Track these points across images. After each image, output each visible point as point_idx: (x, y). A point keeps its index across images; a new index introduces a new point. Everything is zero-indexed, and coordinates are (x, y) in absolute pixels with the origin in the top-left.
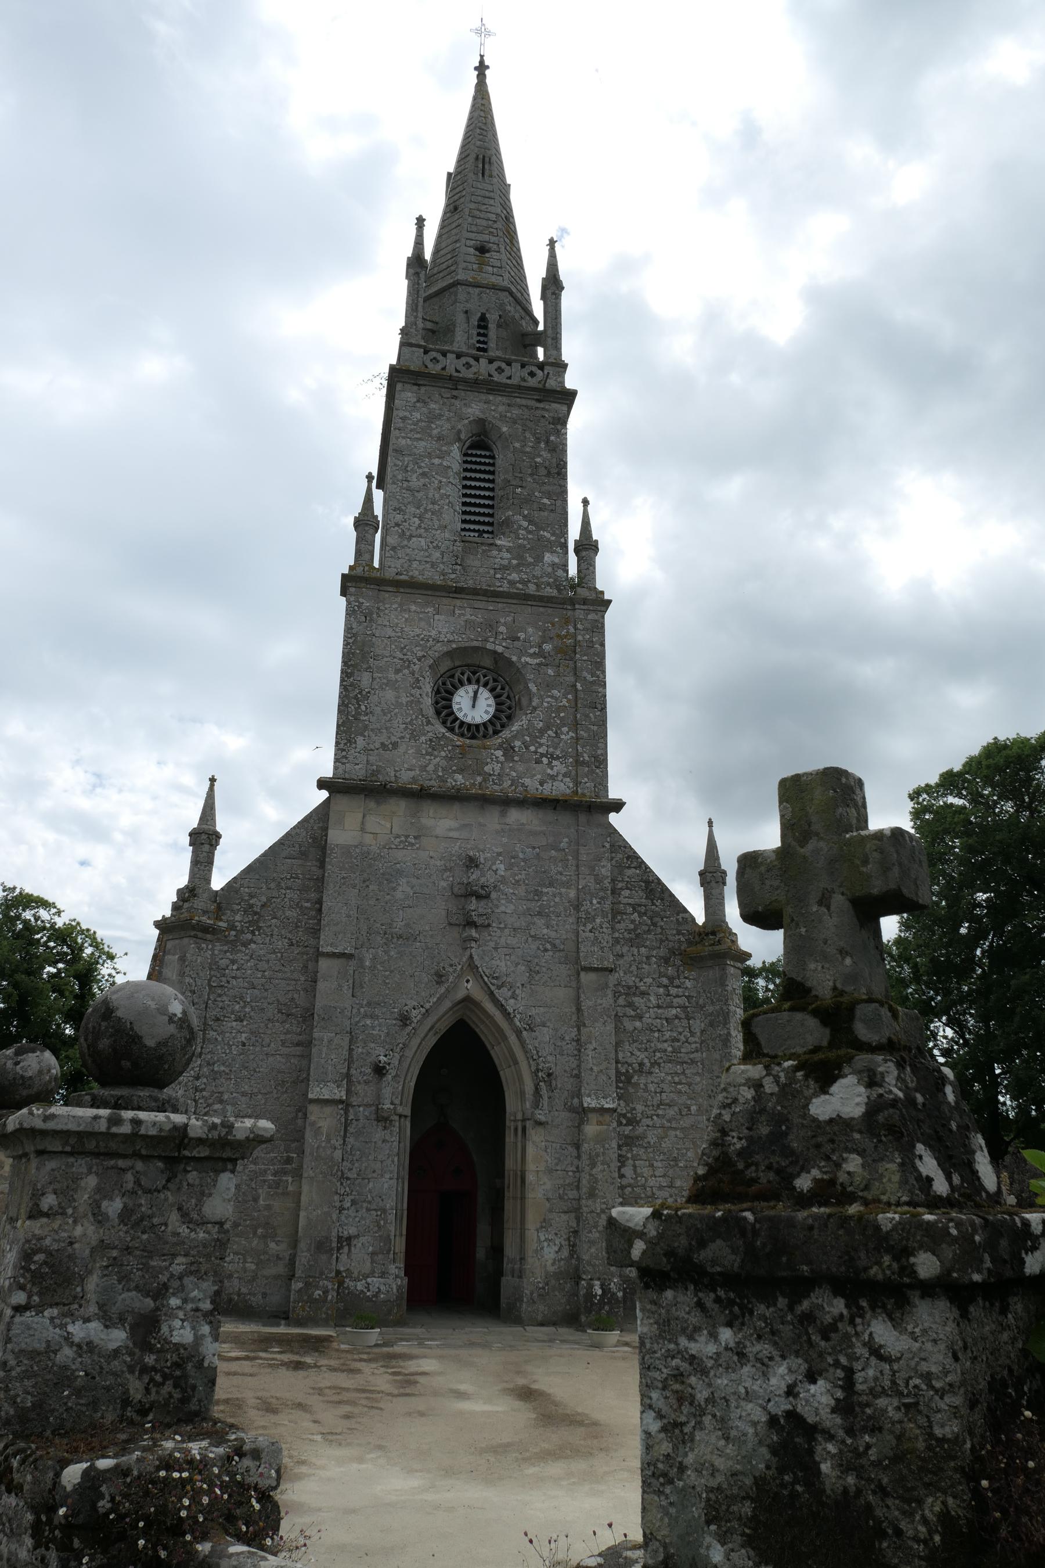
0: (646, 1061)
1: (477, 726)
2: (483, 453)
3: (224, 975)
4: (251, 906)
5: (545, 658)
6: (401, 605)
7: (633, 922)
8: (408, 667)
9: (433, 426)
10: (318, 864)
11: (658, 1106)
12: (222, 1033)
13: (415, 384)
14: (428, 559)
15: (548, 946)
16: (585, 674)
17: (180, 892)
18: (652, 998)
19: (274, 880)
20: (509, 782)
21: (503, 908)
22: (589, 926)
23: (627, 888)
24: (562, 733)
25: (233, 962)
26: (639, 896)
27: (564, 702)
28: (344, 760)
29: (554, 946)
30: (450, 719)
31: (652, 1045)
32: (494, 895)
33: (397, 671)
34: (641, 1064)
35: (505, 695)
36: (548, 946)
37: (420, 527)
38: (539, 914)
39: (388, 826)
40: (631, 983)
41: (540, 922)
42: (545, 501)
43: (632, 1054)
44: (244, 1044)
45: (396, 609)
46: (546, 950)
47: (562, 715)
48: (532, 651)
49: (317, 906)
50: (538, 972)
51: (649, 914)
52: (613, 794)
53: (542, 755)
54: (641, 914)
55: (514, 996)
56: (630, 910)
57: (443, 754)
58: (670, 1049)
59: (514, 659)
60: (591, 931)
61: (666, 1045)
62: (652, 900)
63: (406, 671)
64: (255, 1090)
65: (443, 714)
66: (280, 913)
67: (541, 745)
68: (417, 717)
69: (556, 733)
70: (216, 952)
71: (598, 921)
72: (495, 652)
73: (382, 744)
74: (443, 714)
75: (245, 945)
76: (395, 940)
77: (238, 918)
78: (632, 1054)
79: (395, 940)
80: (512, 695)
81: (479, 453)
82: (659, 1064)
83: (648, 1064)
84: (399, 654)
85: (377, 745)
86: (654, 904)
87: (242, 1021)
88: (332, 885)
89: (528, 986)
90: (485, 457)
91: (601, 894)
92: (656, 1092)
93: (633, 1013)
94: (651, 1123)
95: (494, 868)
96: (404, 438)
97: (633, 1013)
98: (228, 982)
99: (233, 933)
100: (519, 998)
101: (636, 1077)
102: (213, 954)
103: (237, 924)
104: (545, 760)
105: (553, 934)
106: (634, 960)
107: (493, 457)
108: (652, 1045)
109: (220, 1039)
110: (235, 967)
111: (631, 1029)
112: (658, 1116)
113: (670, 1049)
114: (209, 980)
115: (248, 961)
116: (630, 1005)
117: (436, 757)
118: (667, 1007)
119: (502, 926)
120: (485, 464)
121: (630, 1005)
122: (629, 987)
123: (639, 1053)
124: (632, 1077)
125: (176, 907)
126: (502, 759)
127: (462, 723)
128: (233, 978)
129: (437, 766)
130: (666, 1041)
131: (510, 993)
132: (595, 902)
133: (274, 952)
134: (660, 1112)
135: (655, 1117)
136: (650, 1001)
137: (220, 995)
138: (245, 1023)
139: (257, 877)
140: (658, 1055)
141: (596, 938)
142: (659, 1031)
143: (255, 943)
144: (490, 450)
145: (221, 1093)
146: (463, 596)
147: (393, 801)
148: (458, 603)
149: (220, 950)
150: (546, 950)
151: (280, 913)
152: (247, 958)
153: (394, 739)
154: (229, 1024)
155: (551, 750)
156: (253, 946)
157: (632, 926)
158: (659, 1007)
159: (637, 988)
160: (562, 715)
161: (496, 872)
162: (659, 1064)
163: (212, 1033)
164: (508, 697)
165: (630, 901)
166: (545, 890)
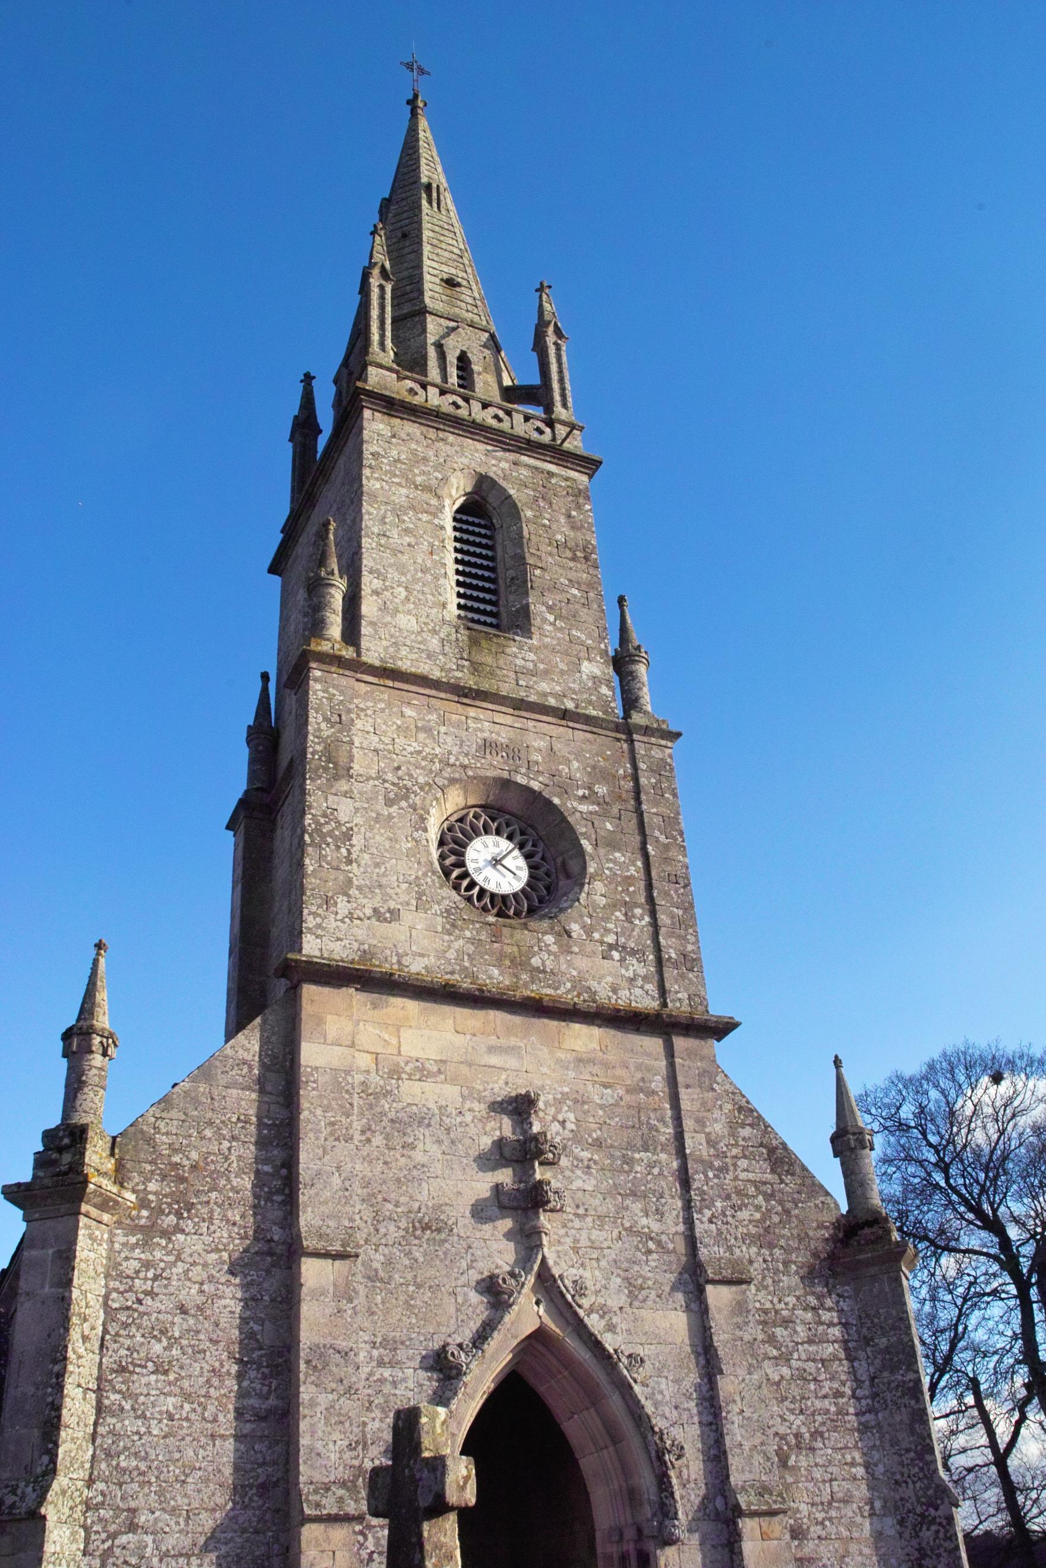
0: (804, 1430)
1: (504, 898)
2: (477, 521)
3: (130, 1289)
4: (176, 1166)
5: (598, 804)
6: (389, 704)
7: (758, 1208)
8: (406, 797)
9: (416, 471)
10: (281, 1100)
11: (830, 1503)
12: (135, 1397)
13: (388, 415)
14: (422, 647)
15: (651, 1245)
16: (657, 833)
17: (49, 1136)
18: (799, 1329)
19: (210, 1123)
20: (569, 985)
21: (578, 1183)
22: (708, 1213)
23: (745, 1157)
24: (634, 916)
25: (147, 1265)
26: (761, 1171)
27: (632, 871)
28: (319, 932)
29: (659, 1243)
30: (465, 883)
31: (809, 1403)
32: (564, 1162)
33: (389, 802)
34: (798, 1436)
35: (540, 855)
36: (651, 1245)
37: (407, 599)
38: (633, 1194)
39: (394, 1041)
40: (768, 1305)
41: (637, 1207)
42: (575, 591)
43: (784, 1420)
44: (171, 1418)
45: (383, 710)
46: (649, 1252)
47: (631, 889)
48: (580, 793)
49: (284, 1172)
50: (642, 1288)
51: (778, 1196)
52: (718, 1009)
53: (612, 947)
54: (768, 1197)
55: (611, 1328)
56: (752, 1190)
57: (468, 934)
58: (833, 1409)
59: (556, 801)
60: (711, 1221)
61: (826, 1402)
62: (780, 1176)
63: (404, 804)
64: (195, 1504)
65: (454, 874)
66: (223, 1182)
67: (607, 931)
68: (425, 875)
69: (626, 914)
70: (117, 1246)
71: (718, 1204)
72: (528, 789)
73: (375, 910)
74: (454, 874)
75: (167, 1234)
76: (418, 1233)
77: (152, 1186)
78: (784, 1420)
79: (418, 1233)
80: (548, 855)
81: (471, 519)
82: (821, 1434)
83: (807, 1435)
84: (389, 776)
85: (368, 912)
86: (782, 1181)
87: (166, 1373)
88: (311, 1135)
89: (628, 1310)
90: (479, 525)
91: (717, 1163)
92: (824, 1481)
93: (775, 1353)
94: (823, 1534)
95: (561, 1118)
96: (377, 479)
97: (775, 1353)
98: (140, 1302)
99: (145, 1213)
100: (618, 1330)
101: (793, 1457)
102: (111, 1249)
103: (151, 1197)
104: (616, 955)
105: (656, 1227)
106: (768, 1269)
107: (491, 527)
108: (809, 1403)
109: (127, 1407)
110: (150, 1275)
111: (777, 1378)
112: (830, 1519)
113: (833, 1409)
114: (106, 1297)
115: (174, 1264)
116: (771, 1340)
117: (458, 938)
118: (821, 1342)
119: (581, 1211)
120: (479, 535)
121: (771, 1340)
122: (766, 1312)
123: (792, 1418)
124: (788, 1457)
125: (41, 1161)
126: (554, 948)
127: (482, 891)
128: (147, 1293)
129: (460, 952)
130: (825, 1397)
131: (603, 1323)
132: (711, 1174)
133: (217, 1250)
134: (833, 1513)
135: (827, 1523)
136: (795, 1332)
137: (126, 1326)
138: (172, 1377)
139: (183, 1117)
140: (819, 1418)
141: (720, 1232)
142: (815, 1379)
143: (183, 1231)
144: (490, 518)
145: (133, 1511)
146: (478, 703)
147: (398, 1002)
148: (472, 712)
149: (124, 1245)
150: (649, 1252)
151: (223, 1182)
152: (172, 1258)
153: (392, 905)
154: (144, 1380)
155: (622, 940)
156: (181, 1237)
157: (758, 1216)
158: (810, 1342)
159: (777, 1312)
160: (631, 889)
161: (563, 1123)
162: (821, 1434)
163: (114, 1397)
164: (543, 858)
165: (751, 1176)
166: (637, 1156)
